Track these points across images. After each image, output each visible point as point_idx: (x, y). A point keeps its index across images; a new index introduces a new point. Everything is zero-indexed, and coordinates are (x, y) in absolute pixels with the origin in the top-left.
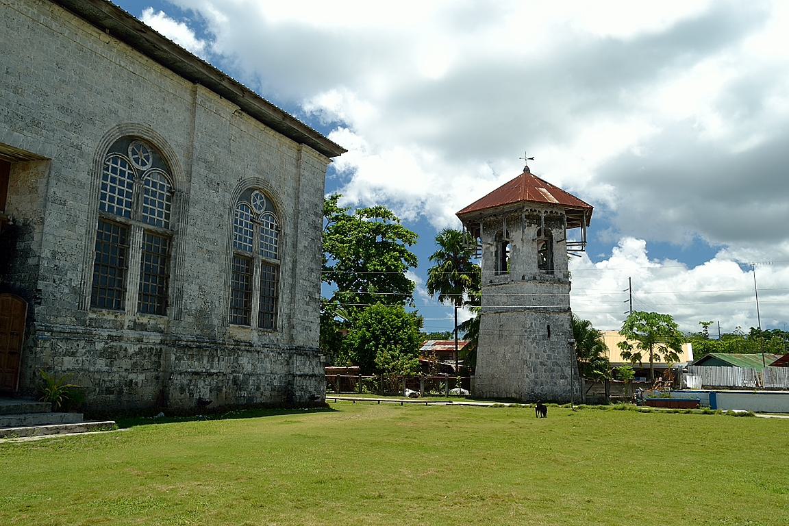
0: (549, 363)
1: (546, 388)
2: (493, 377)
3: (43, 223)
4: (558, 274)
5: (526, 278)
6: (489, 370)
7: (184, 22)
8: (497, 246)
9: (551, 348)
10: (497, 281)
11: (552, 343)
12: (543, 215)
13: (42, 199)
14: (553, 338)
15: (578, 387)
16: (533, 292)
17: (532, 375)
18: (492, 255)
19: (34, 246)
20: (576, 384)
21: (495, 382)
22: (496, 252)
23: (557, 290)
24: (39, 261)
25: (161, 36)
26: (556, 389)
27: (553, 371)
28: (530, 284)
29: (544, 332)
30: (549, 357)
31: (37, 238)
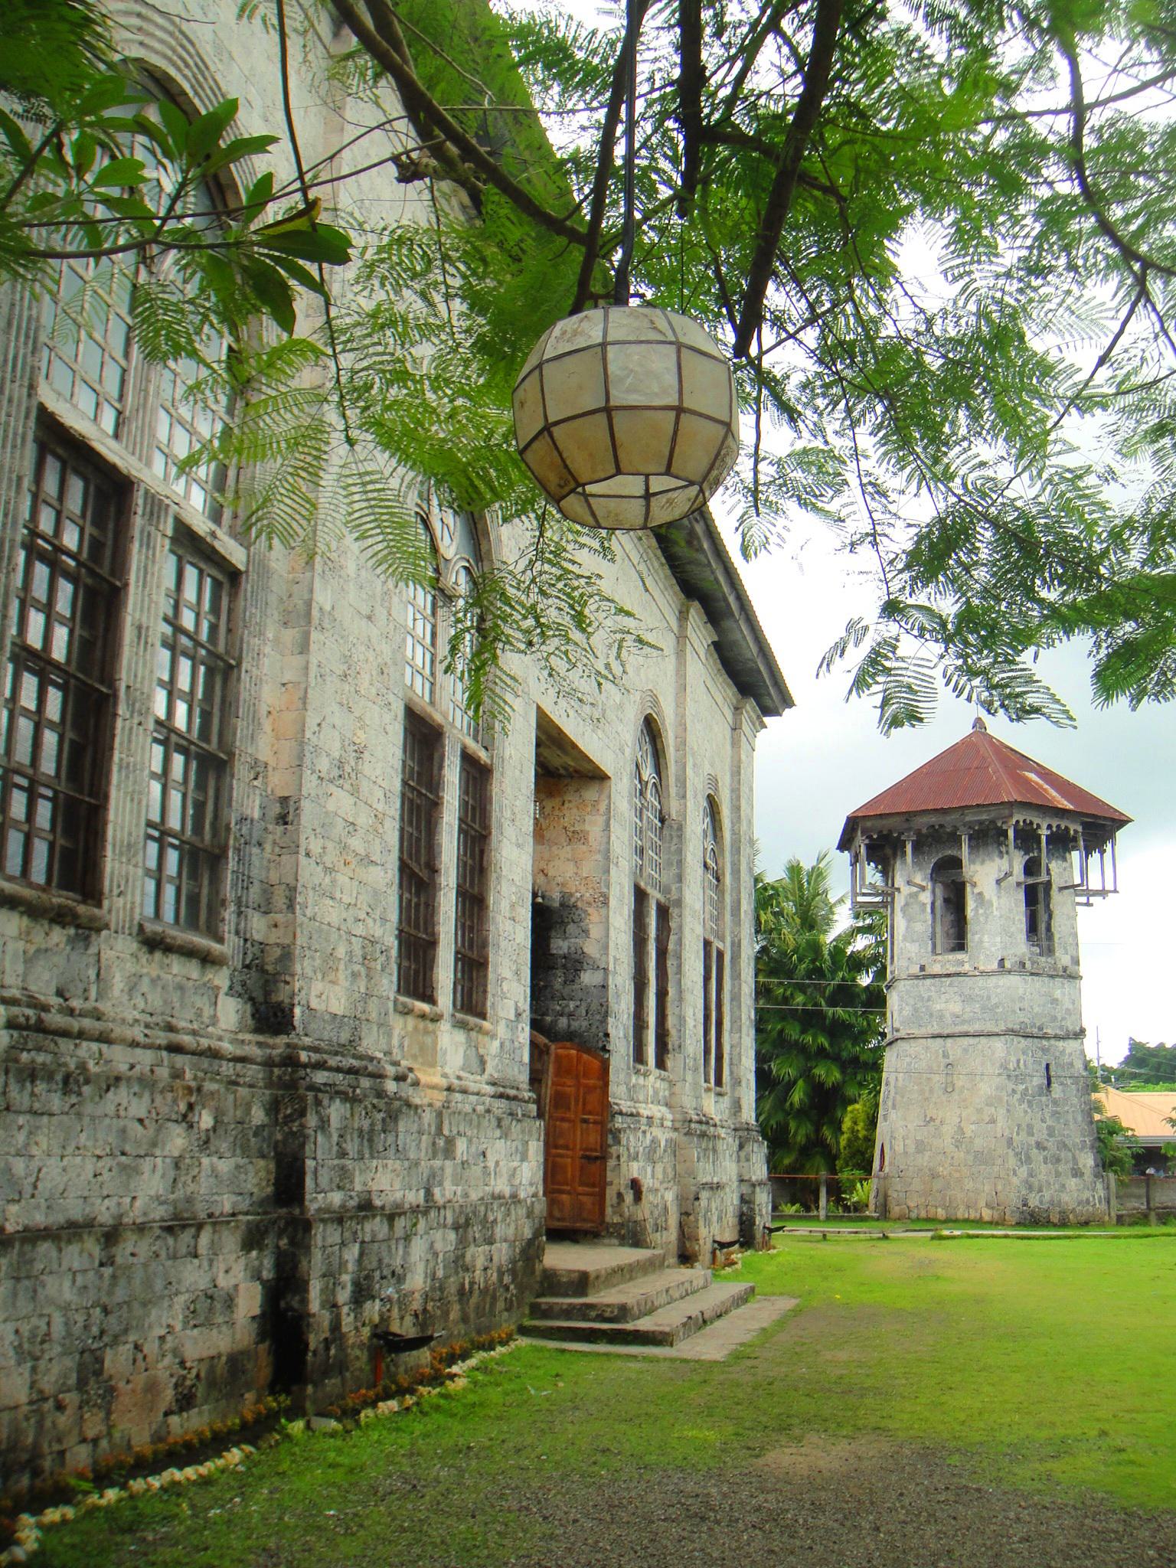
0: (1051, 1144)
1: (1047, 1195)
2: (934, 1176)
3: (606, 903)
4: (1063, 959)
5: (1008, 965)
6: (924, 1160)
7: (705, 503)
8: (933, 892)
9: (1055, 1113)
10: (937, 969)
11: (1055, 1102)
12: (1044, 832)
13: (599, 857)
14: (1057, 1090)
15: (1102, 1193)
16: (1020, 994)
17: (1023, 1172)
18: (924, 911)
19: (591, 949)
20: (1099, 1186)
21: (938, 1185)
22: (933, 904)
23: (1060, 990)
24: (606, 979)
25: (61, 425)
26: (1065, 1198)
27: (1058, 1160)
28: (1014, 980)
29: (1039, 1080)
30: (1051, 1131)
31: (595, 931)
